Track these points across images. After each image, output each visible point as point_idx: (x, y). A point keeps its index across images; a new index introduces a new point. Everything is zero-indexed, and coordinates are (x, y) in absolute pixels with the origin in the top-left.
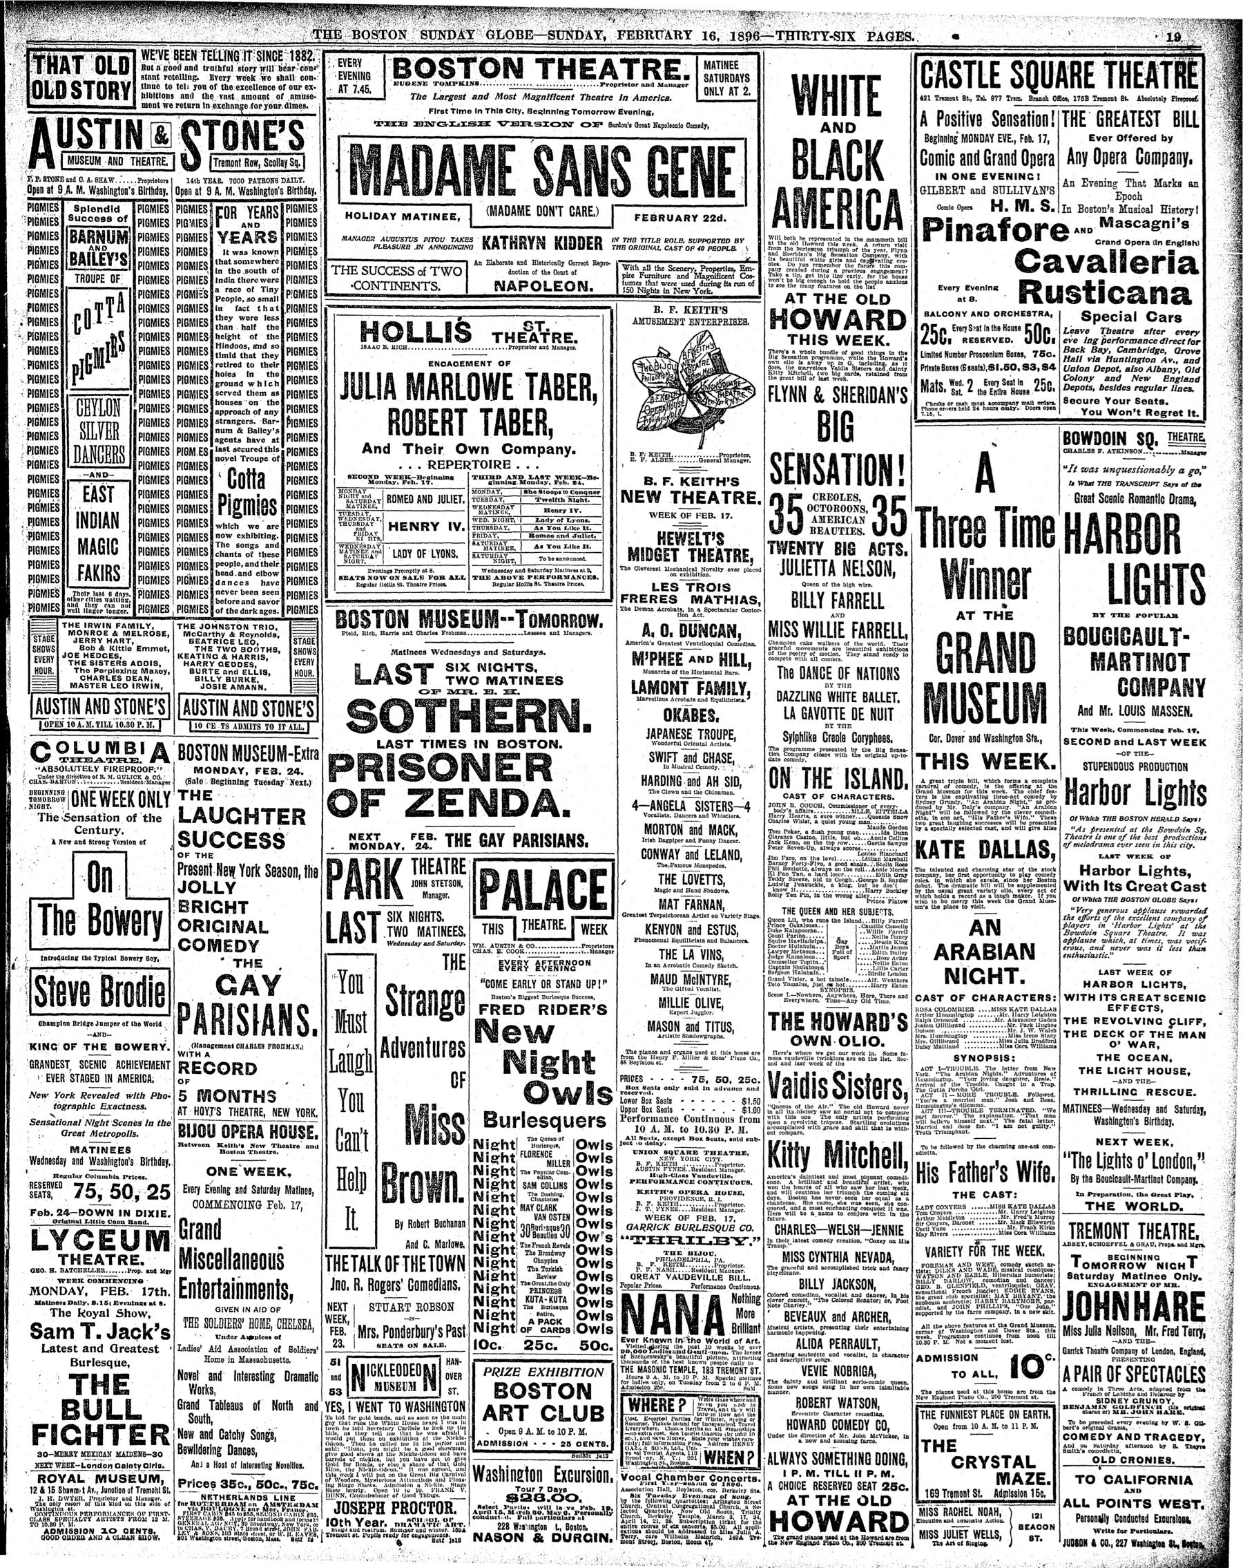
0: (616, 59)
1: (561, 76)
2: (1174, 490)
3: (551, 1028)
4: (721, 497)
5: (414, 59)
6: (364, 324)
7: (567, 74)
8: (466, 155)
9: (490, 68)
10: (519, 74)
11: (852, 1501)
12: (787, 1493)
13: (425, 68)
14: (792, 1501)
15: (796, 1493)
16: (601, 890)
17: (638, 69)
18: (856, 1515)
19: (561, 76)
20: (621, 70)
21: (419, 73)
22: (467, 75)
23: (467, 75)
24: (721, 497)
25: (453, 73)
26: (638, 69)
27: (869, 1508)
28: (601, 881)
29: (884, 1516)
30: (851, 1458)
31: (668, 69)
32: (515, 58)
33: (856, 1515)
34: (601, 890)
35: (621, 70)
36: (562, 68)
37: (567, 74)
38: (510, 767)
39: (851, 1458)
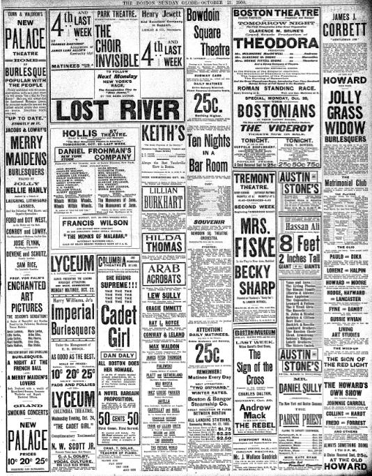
0: (299, 10)
1: (246, 47)
2: (215, 395)
3: (269, 266)
4: (256, 187)
5: (240, 10)
6: (64, 131)
7: (249, 46)
8: (150, 115)
9: (262, 13)
10: (271, 15)
11: (350, 460)
12: (330, 458)
13: (244, 13)
14: (331, 460)
15: (333, 458)
16: (246, 272)
17: (306, 12)
18: (350, 465)
19: (246, 47)
20: (301, 13)
21: (242, 15)
22: (256, 15)
23: (256, 15)
24: (256, 187)
25: (252, 14)
26: (306, 12)
27: (355, 462)
28: (246, 269)
29: (359, 465)
30: (349, 445)
31: (315, 12)
32: (270, 10)
33: (350, 465)
34: (246, 272)
35: (301, 13)
36: (283, 13)
37: (249, 46)
38: (261, 43)
39: (349, 445)
